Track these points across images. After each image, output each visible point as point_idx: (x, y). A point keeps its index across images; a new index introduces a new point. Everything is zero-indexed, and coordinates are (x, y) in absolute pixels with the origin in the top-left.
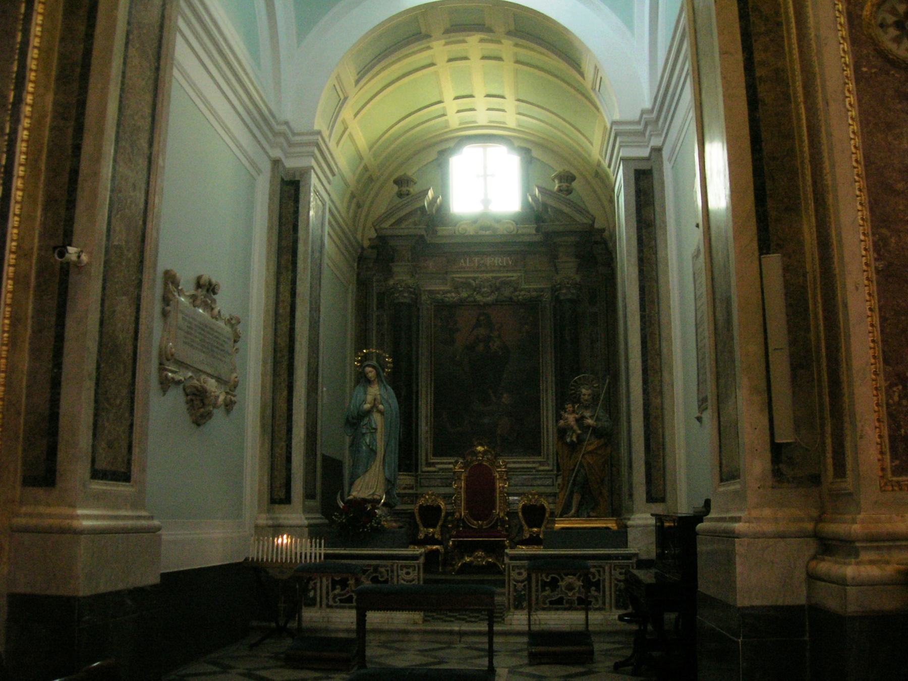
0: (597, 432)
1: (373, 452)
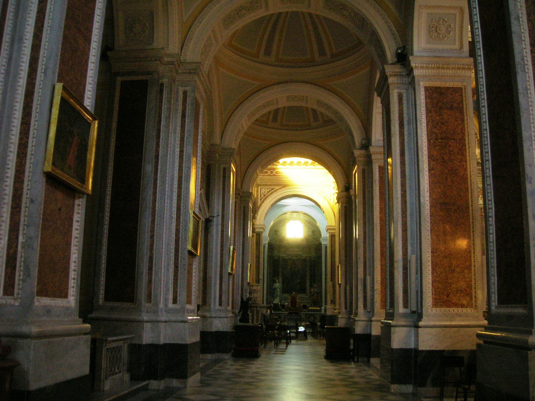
0: (317, 293)
1: (277, 295)
